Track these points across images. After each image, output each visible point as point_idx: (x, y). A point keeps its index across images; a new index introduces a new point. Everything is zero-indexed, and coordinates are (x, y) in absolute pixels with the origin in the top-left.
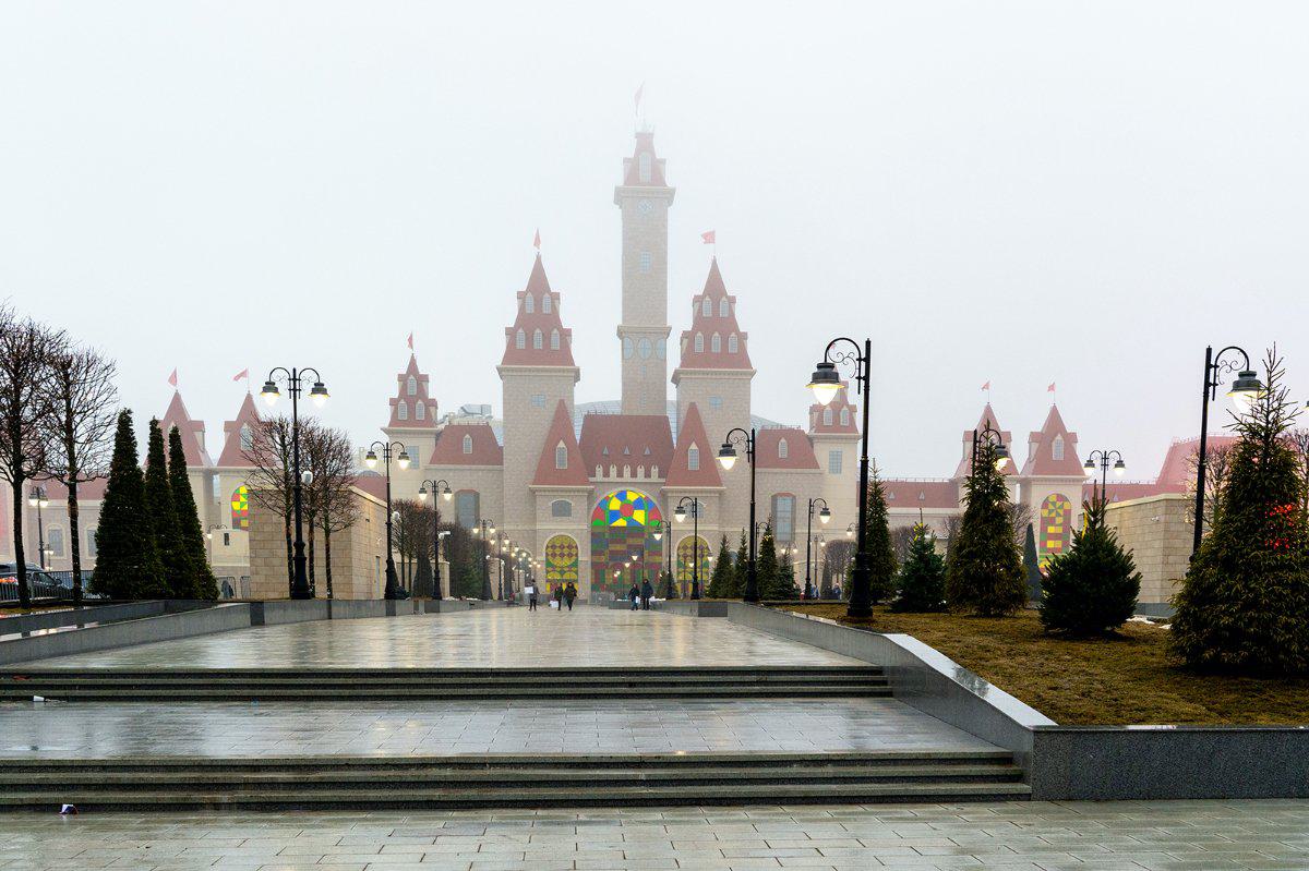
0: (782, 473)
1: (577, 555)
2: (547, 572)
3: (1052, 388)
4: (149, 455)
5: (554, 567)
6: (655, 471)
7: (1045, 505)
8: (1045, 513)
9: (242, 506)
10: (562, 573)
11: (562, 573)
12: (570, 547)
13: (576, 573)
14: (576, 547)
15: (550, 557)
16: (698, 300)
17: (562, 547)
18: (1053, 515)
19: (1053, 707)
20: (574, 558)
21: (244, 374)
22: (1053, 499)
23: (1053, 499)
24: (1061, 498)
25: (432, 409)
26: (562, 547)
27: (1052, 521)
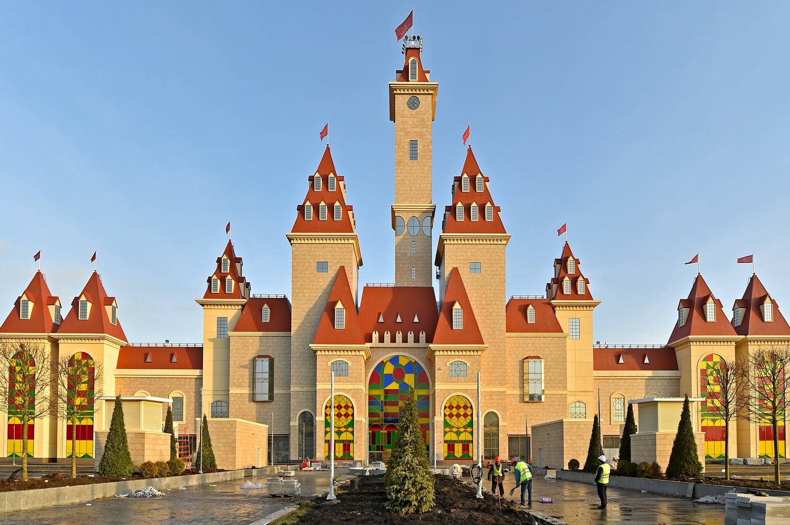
0: (624, 413)
1: (353, 415)
2: (445, 433)
3: (37, 257)
4: (681, 421)
5: (451, 427)
10: (458, 433)
11: (458, 433)
12: (347, 407)
13: (352, 433)
15: (447, 418)
17: (458, 407)
19: (70, 483)
20: (350, 418)
21: (414, 156)
22: (79, 357)
23: (79, 357)
24: (85, 356)
25: (238, 265)
26: (458, 407)
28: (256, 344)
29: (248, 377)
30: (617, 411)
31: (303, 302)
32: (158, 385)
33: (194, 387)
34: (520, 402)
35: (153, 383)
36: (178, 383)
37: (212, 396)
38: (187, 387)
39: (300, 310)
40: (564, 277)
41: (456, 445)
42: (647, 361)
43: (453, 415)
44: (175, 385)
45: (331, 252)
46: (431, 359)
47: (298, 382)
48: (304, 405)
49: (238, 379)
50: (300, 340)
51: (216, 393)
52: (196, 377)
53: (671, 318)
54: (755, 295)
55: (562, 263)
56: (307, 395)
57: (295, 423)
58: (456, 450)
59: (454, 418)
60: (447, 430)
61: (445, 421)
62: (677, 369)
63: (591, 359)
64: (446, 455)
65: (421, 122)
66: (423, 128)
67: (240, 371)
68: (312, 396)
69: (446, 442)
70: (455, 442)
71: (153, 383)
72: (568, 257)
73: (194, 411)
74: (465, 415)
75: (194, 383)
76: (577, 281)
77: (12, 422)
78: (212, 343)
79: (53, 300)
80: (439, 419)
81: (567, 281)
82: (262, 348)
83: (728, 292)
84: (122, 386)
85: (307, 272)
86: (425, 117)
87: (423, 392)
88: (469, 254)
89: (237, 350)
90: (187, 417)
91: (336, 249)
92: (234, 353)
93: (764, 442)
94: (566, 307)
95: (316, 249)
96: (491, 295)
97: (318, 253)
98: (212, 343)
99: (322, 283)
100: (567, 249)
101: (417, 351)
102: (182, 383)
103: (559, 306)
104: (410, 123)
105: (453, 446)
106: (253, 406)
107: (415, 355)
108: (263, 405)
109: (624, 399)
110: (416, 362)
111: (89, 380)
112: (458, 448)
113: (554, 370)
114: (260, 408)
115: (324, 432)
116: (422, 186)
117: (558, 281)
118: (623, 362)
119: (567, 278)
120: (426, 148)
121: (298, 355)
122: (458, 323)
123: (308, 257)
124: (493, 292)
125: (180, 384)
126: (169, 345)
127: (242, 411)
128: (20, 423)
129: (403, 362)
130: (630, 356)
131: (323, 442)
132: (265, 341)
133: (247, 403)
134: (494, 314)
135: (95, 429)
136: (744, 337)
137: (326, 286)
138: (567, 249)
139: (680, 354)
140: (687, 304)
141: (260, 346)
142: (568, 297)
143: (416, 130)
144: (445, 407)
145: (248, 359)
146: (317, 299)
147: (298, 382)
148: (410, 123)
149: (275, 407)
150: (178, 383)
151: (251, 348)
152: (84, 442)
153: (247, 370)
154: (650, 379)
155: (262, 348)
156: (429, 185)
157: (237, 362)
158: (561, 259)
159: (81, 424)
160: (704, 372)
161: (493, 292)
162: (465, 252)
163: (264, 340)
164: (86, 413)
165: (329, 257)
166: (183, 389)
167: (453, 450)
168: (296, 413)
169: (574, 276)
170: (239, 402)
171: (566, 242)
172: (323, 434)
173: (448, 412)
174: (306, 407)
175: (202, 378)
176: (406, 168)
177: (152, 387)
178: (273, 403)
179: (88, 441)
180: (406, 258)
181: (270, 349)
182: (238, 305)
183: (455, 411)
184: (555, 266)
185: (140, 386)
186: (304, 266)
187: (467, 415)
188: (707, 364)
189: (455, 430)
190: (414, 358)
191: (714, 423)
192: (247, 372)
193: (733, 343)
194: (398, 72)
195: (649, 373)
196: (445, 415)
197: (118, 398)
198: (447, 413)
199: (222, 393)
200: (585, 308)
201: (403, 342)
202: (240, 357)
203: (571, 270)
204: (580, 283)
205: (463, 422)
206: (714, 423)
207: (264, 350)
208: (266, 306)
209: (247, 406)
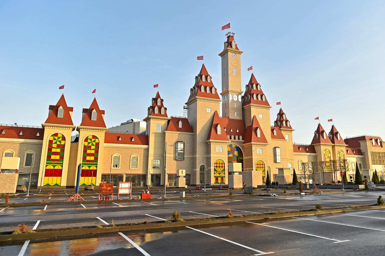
1: (224, 167)
2: (215, 173)
3: (94, 91)
5: (217, 171)
6: (241, 137)
7: (86, 140)
8: (86, 144)
9: (88, 144)
12: (262, 165)
14: (224, 164)
15: (215, 168)
16: (247, 86)
18: (90, 145)
20: (264, 168)
23: (90, 137)
27: (90, 148)
28: (177, 136)
29: (173, 150)
30: (134, 163)
31: (201, 123)
32: (125, 151)
33: (143, 153)
34: (174, 160)
35: (122, 150)
36: (135, 150)
37: (153, 157)
38: (140, 152)
39: (200, 125)
40: (155, 106)
41: (219, 178)
42: (307, 150)
43: (217, 167)
44: (134, 152)
45: (212, 105)
47: (200, 153)
48: (202, 162)
49: (169, 151)
50: (200, 137)
51: (155, 156)
52: (145, 148)
54: (321, 130)
55: (155, 100)
56: (203, 158)
57: (198, 169)
60: (215, 172)
62: (315, 153)
63: (292, 148)
64: (215, 182)
65: (237, 62)
66: (238, 64)
67: (170, 147)
68: (208, 160)
69: (215, 177)
71: (122, 150)
72: (158, 98)
73: (142, 163)
74: (262, 167)
75: (143, 151)
76: (161, 109)
77: (48, 168)
78: (154, 134)
80: (212, 168)
82: (179, 138)
83: (327, 130)
84: (106, 151)
85: (203, 111)
86: (238, 61)
88: (259, 111)
89: (169, 138)
90: (139, 166)
91: (214, 104)
92: (167, 140)
93: (47, 177)
94: (283, 130)
95: (206, 103)
96: (266, 126)
97: (207, 105)
98: (154, 134)
99: (208, 116)
100: (158, 95)
101: (239, 143)
102: (137, 151)
103: (282, 130)
104: (233, 62)
105: (218, 178)
106: (175, 161)
107: (238, 144)
108: (179, 162)
109: (137, 157)
111: (96, 148)
112: (219, 179)
113: (283, 152)
114: (178, 163)
115: (214, 173)
116: (238, 84)
117: (153, 108)
118: (121, 140)
119: (156, 107)
120: (239, 71)
121: (199, 143)
123: (203, 106)
124: (267, 125)
125: (136, 151)
126: (127, 133)
127: (171, 164)
128: (89, 169)
130: (14, 131)
131: (214, 177)
132: (181, 135)
133: (173, 160)
134: (267, 132)
135: (252, 171)
136: (334, 144)
137: (210, 117)
138: (158, 95)
139: (316, 148)
140: (54, 109)
141: (179, 137)
142: (156, 115)
143: (235, 65)
144: (215, 164)
145: (173, 142)
146: (207, 122)
147: (200, 153)
148: (233, 62)
149: (185, 162)
150: (135, 150)
151: (175, 138)
152: (87, 178)
153: (173, 147)
154: (309, 156)
155: (179, 138)
156: (240, 84)
157: (169, 144)
158: (155, 98)
159: (90, 169)
160: (51, 142)
161: (267, 125)
162: (257, 111)
163: (181, 135)
164: (54, 163)
165: (211, 107)
166: (138, 154)
167: (218, 180)
168: (199, 165)
169: (160, 106)
170: (169, 160)
171: (158, 91)
176: (232, 77)
177: (122, 152)
178: (184, 161)
179: (89, 177)
180: (233, 109)
181: (183, 139)
182: (166, 120)
183: (218, 165)
184: (152, 101)
185: (116, 151)
186: (202, 109)
187: (223, 167)
188: (54, 138)
189: (218, 172)
191: (54, 168)
192: (173, 148)
193: (331, 146)
195: (22, 140)
196: (215, 167)
198: (257, 167)
199: (160, 156)
200: (288, 131)
201: (234, 139)
202: (170, 141)
203: (159, 104)
204: (163, 109)
206: (54, 168)
207: (180, 139)
209: (173, 162)
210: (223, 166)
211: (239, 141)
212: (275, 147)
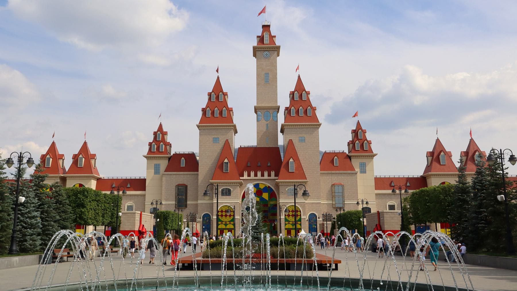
1: (300, 215)
2: (286, 224)
5: (289, 222)
10: (226, 225)
11: (226, 225)
14: (300, 211)
15: (287, 217)
20: (232, 217)
41: (292, 231)
46: (277, 186)
53: (424, 163)
55: (355, 133)
58: (292, 233)
59: (224, 217)
60: (287, 223)
61: (285, 219)
63: (373, 183)
70: (224, 229)
79: (62, 157)
81: (360, 144)
87: (272, 203)
101: (270, 181)
105: (290, 231)
110: (269, 187)
122: (292, 167)
129: (262, 187)
140: (431, 154)
172: (284, 225)
173: (287, 214)
174: (206, 211)
175: (144, 196)
189: (224, 223)
190: (268, 185)
194: (258, 37)
196: (285, 215)
197: (378, 212)
201: (248, 176)
205: (228, 219)
208: (183, 158)
210: (232, 215)
211: (249, 178)
212: (334, 185)
